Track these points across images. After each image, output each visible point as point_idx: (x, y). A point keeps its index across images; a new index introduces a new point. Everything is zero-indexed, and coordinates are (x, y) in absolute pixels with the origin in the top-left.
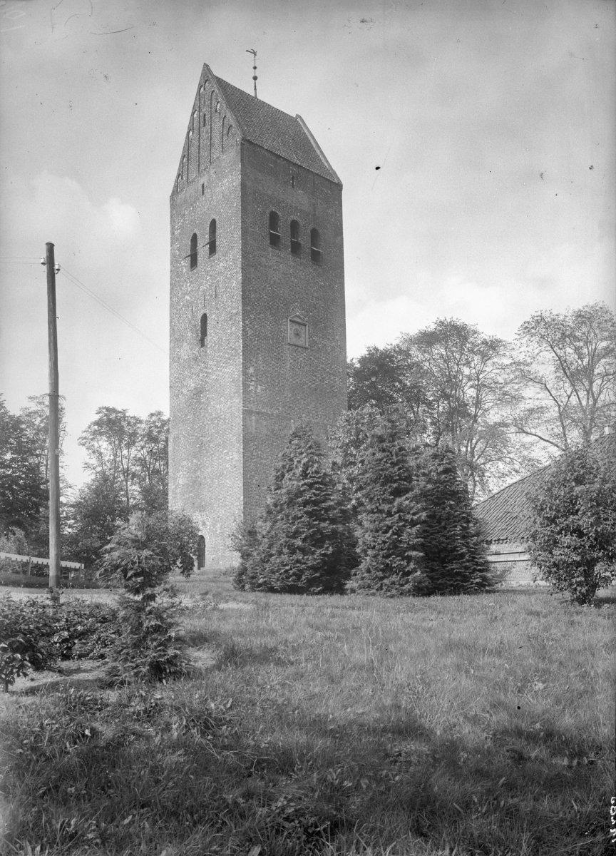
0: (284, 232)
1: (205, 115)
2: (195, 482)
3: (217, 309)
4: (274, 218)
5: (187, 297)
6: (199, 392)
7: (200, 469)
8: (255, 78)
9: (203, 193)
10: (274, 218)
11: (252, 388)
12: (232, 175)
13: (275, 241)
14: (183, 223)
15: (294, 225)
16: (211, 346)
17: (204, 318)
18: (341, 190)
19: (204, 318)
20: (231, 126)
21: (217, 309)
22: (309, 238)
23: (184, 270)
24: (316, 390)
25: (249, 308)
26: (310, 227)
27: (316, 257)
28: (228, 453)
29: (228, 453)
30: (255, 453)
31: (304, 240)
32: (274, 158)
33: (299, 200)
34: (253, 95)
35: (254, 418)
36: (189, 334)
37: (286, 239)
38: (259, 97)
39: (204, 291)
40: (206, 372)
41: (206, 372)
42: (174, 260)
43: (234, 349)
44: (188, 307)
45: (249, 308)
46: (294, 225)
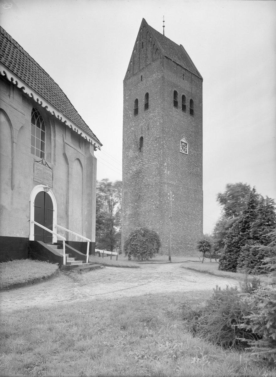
0: (179, 100)
1: (143, 43)
2: (136, 213)
3: (149, 135)
4: (175, 93)
5: (133, 129)
6: (138, 173)
7: (139, 208)
8: (164, 27)
9: (142, 80)
10: (175, 93)
11: (166, 172)
12: (158, 72)
13: (176, 104)
14: (130, 93)
15: (184, 97)
16: (145, 152)
17: (142, 139)
18: (202, 82)
19: (142, 139)
20: (158, 49)
21: (149, 135)
22: (189, 104)
23: (131, 116)
24: (190, 173)
25: (165, 135)
26: (190, 98)
27: (192, 112)
28: (154, 201)
29: (154, 201)
30: (166, 202)
31: (187, 104)
32: (176, 65)
33: (184, 87)
34: (162, 34)
35: (166, 185)
36: (133, 146)
37: (180, 104)
38: (165, 35)
39: (142, 126)
40: (142, 164)
41: (142, 164)
42: (125, 110)
43: (157, 154)
44: (133, 133)
45: (165, 135)
46: (184, 97)
